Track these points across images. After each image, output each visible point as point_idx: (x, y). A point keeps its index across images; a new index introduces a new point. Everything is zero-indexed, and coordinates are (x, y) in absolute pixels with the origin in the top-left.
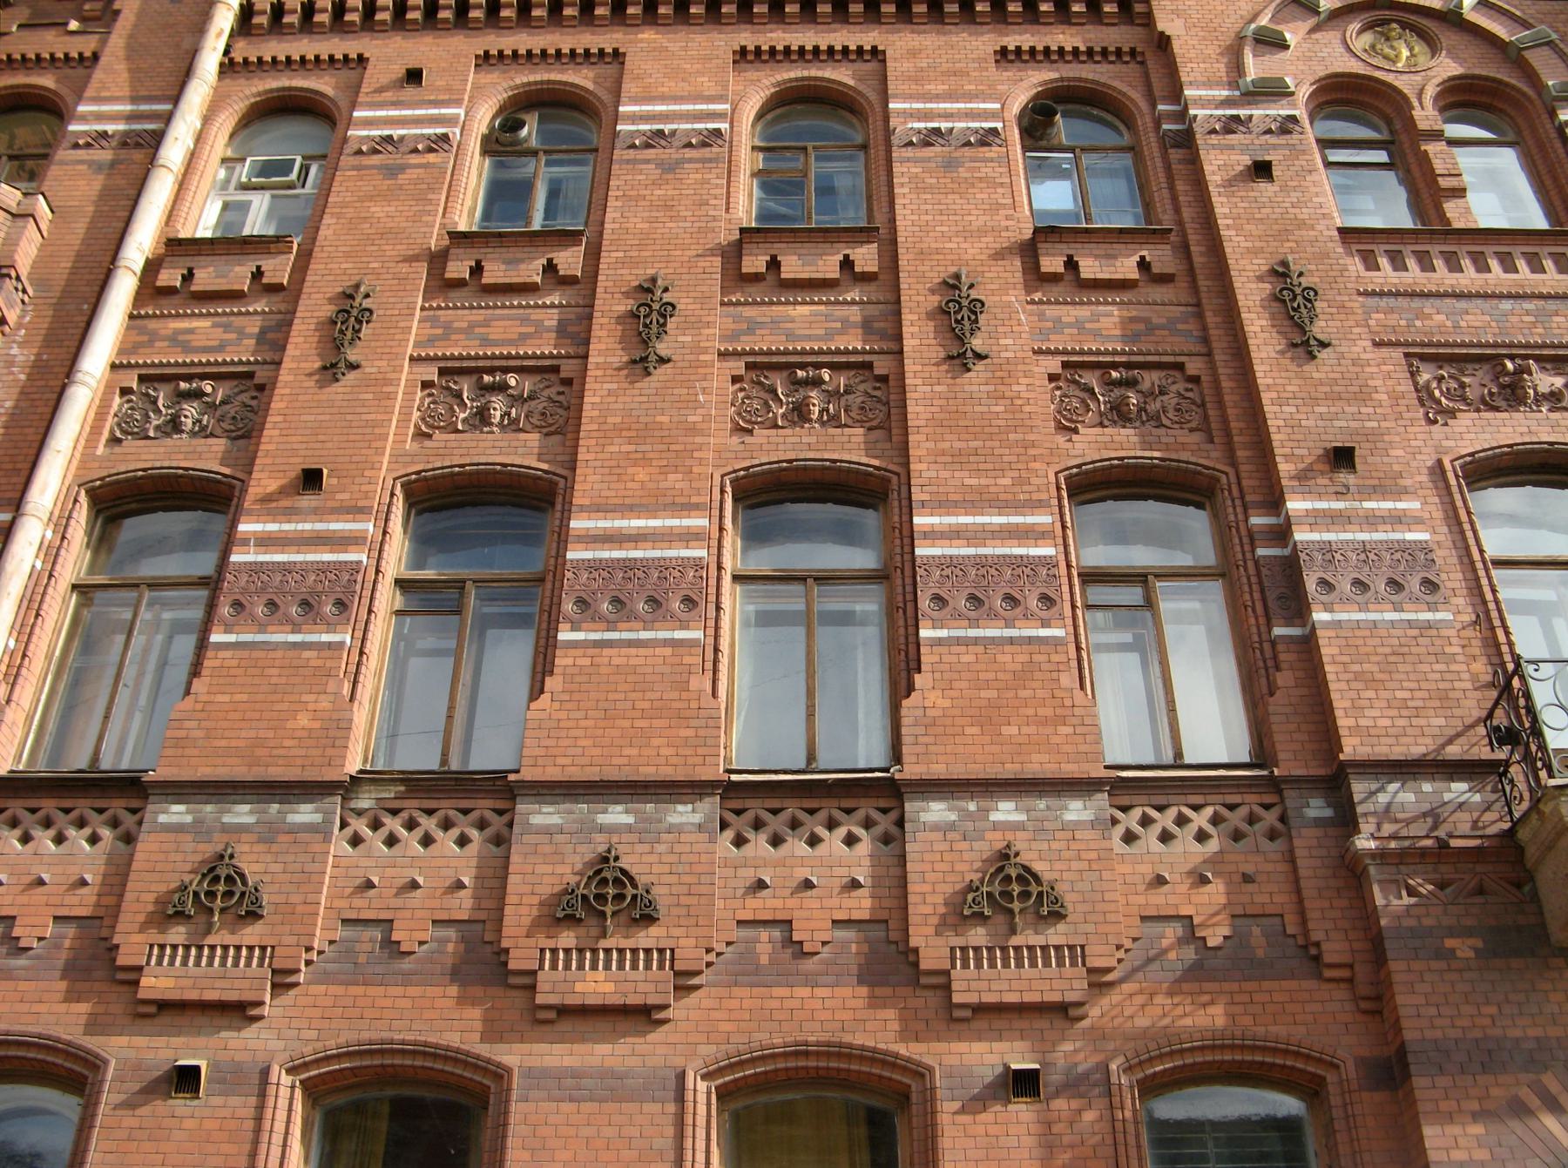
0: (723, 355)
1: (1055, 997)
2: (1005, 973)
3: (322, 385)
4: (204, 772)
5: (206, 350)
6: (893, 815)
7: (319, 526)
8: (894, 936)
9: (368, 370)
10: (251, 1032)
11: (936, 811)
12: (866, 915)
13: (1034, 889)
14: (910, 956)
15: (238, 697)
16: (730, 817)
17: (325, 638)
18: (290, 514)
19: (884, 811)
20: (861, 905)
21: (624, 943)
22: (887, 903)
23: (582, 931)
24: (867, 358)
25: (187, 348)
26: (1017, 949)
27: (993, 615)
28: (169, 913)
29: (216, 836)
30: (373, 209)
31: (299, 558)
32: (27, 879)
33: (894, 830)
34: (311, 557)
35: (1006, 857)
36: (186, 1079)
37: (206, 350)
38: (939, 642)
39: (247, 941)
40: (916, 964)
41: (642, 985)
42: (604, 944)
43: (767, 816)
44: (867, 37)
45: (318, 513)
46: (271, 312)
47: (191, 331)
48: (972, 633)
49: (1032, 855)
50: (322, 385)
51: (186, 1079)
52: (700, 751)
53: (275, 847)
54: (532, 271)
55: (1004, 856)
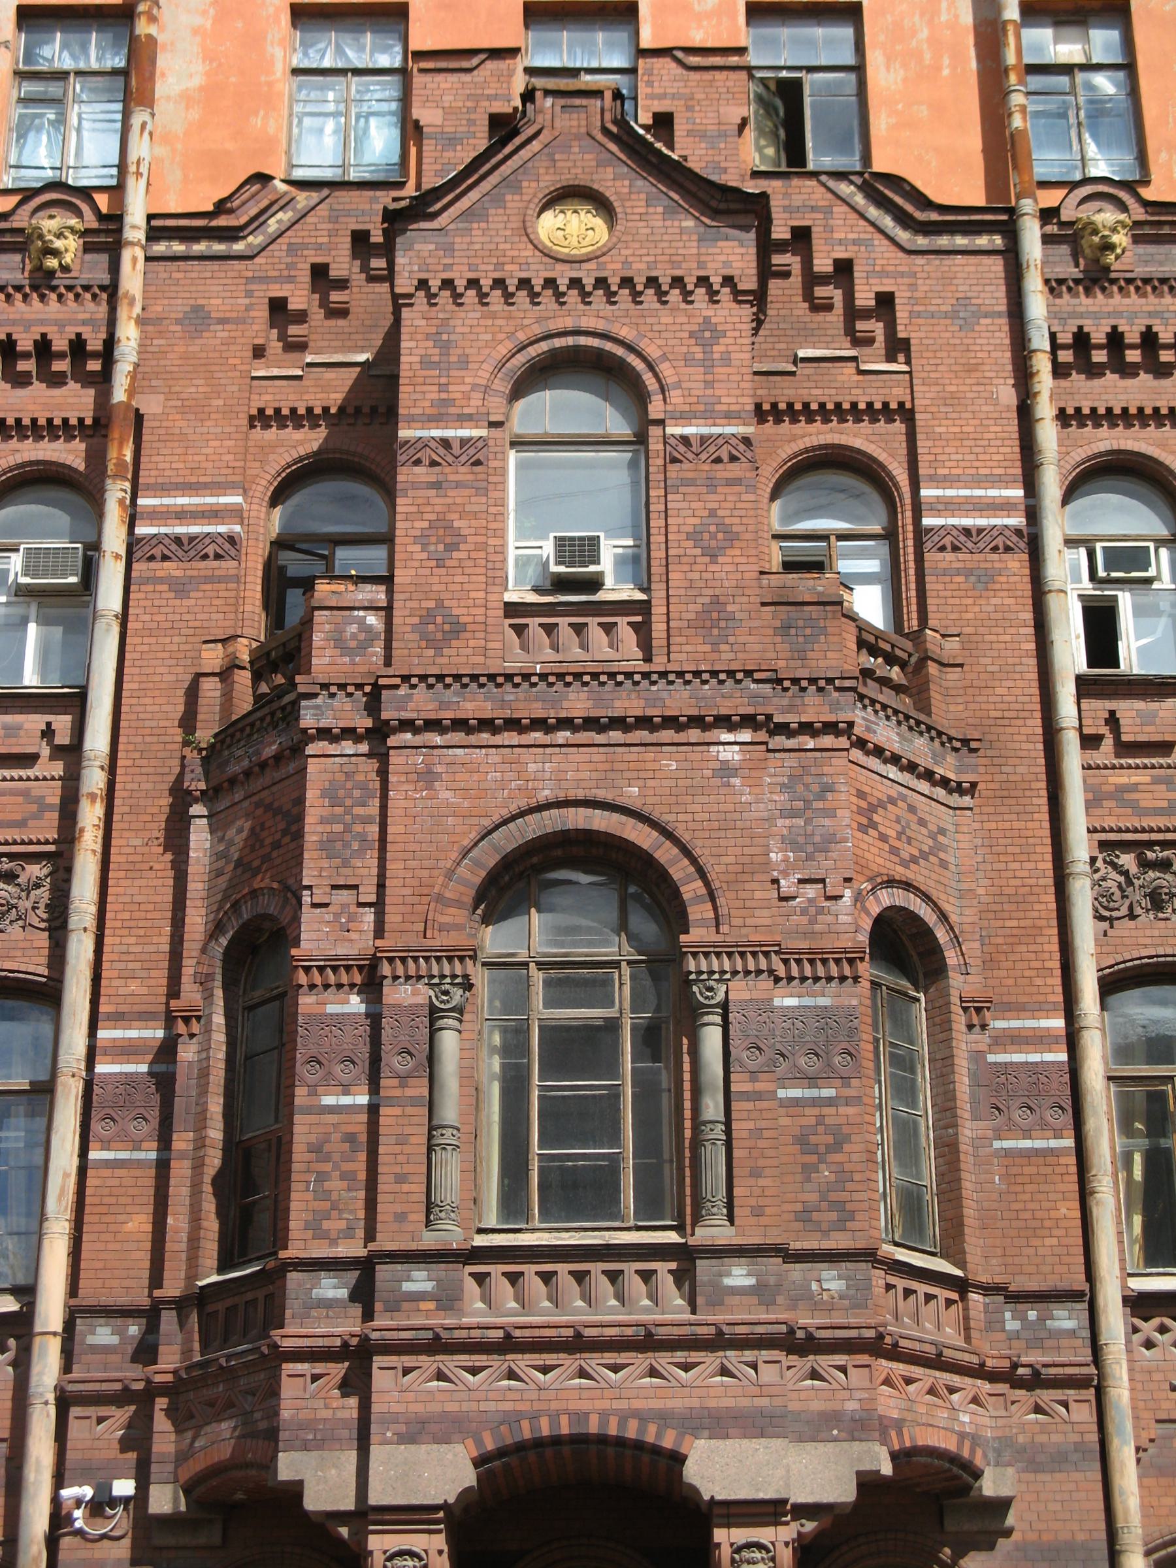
47: (1134, 788)
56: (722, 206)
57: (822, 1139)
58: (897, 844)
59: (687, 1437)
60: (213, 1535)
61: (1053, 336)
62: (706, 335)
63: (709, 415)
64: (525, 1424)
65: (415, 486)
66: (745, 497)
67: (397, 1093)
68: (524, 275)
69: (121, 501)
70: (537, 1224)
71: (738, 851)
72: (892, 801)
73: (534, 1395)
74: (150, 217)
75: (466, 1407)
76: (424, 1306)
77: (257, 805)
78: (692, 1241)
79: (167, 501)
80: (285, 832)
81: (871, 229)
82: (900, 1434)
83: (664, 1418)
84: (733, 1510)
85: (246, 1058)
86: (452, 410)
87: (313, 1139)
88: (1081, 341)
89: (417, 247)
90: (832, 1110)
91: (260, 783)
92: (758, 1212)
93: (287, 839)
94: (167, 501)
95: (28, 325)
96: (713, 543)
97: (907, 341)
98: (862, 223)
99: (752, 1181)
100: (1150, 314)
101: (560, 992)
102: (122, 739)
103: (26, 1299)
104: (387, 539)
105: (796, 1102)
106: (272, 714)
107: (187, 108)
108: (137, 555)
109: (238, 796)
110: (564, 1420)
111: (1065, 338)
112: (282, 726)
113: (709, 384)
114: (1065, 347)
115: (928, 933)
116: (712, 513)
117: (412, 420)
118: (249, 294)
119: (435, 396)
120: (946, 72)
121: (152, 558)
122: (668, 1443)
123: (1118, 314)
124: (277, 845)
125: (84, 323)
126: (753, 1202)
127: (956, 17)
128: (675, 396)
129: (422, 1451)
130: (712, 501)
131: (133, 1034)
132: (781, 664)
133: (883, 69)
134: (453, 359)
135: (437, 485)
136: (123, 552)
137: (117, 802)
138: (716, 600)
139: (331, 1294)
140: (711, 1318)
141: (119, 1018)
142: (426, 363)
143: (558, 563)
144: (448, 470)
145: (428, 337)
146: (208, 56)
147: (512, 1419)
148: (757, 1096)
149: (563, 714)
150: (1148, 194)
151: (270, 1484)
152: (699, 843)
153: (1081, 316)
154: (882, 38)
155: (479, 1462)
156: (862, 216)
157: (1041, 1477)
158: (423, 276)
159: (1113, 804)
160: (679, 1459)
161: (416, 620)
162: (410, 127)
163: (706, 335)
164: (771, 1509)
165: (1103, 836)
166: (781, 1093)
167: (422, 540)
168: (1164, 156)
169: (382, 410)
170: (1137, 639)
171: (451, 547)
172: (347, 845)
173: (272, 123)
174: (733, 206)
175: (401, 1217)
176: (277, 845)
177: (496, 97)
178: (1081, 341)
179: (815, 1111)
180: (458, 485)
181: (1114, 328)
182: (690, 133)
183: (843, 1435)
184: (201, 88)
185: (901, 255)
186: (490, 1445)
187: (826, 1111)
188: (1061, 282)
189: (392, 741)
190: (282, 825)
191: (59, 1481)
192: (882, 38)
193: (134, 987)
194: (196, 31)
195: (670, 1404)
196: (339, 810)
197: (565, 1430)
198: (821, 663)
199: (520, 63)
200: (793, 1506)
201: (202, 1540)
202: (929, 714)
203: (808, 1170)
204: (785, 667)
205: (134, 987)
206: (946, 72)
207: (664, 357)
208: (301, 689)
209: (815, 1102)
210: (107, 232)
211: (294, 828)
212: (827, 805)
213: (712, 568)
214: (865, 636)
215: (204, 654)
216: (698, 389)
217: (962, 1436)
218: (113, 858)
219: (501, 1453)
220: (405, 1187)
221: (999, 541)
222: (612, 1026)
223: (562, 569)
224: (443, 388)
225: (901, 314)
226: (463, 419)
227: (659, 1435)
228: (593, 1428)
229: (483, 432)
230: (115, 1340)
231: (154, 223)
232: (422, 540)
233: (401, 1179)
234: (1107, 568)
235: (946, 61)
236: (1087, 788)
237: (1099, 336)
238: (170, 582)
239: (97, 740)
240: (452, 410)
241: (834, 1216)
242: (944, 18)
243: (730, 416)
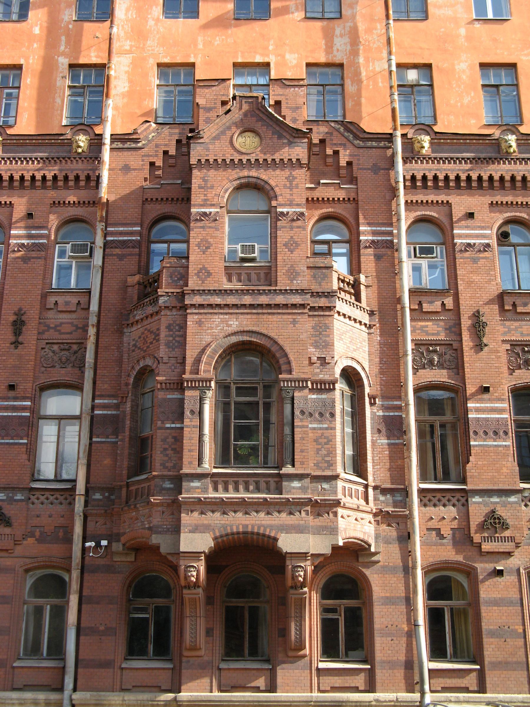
0: (503, 341)
1: (507, 550)
2: (505, 544)
3: (477, 352)
4: (501, 487)
5: (433, 334)
6: (465, 498)
7: (492, 405)
8: (466, 533)
9: (491, 346)
10: (512, 559)
11: (477, 499)
12: (456, 527)
13: (502, 521)
14: (471, 539)
15: (484, 463)
16: (423, 498)
17: (504, 443)
18: (481, 401)
19: (462, 497)
20: (455, 524)
21: (502, 535)
22: (463, 523)
23: (489, 532)
24: (451, 342)
25: (428, 334)
26: (498, 537)
27: (490, 438)
28: (482, 527)
29: (490, 505)
30: (474, 278)
31: (489, 416)
32: (439, 518)
33: (465, 503)
34: (493, 416)
35: (494, 512)
36: (500, 573)
37: (433, 334)
38: (476, 446)
39: (507, 535)
40: (472, 541)
41: (507, 547)
42: (497, 535)
43: (451, 498)
44: (442, 198)
45: (490, 400)
46: (450, 319)
47: (427, 326)
48: (485, 443)
49: (501, 512)
50: (477, 352)
51: (500, 573)
52: (22, 472)
53: (507, 508)
54: (437, 306)
55: (493, 512)
56: (297, 135)
57: (323, 441)
58: (349, 345)
59: (279, 533)
60: (131, 558)
61: (404, 177)
62: (291, 179)
63: (291, 205)
64: (229, 528)
65: (196, 227)
66: (302, 232)
67: (189, 424)
68: (232, 158)
69: (102, 229)
70: (233, 465)
71: (298, 348)
72: (347, 331)
73: (232, 519)
74: (112, 135)
75: (210, 522)
76: (197, 490)
77: (146, 329)
78: (281, 472)
79: (116, 229)
80: (154, 339)
81: (345, 140)
82: (345, 533)
83: (271, 527)
84: (293, 555)
85: (142, 410)
86: (208, 203)
87: (163, 437)
88: (413, 178)
89: (198, 148)
90: (326, 431)
91: (145, 322)
92: (302, 463)
93: (155, 341)
94: (116, 229)
95: (72, 170)
96: (292, 247)
97: (356, 178)
98: (343, 138)
99: (301, 454)
100: (437, 170)
101: (241, 391)
102: (102, 307)
103: (74, 484)
104: (187, 242)
105: (314, 429)
106: (150, 301)
107: (123, 98)
108: (107, 246)
109: (139, 326)
110: (241, 527)
111: (408, 177)
112: (153, 305)
113: (291, 195)
114: (408, 180)
115: (358, 374)
116: (292, 237)
117: (195, 205)
118: (143, 161)
119: (203, 198)
120: (371, 87)
121: (112, 248)
122: (272, 534)
123: (424, 169)
124: (151, 343)
125: (90, 170)
126: (301, 460)
127: (375, 68)
128: (280, 199)
129: (197, 535)
130: (292, 233)
131: (106, 401)
132: (312, 287)
133: (350, 86)
134: (209, 186)
135: (203, 227)
136: (102, 246)
137: (101, 327)
138: (292, 266)
139: (168, 486)
140: (287, 496)
141: (101, 396)
142: (200, 187)
143: (242, 253)
144: (207, 222)
145: (201, 178)
146: (130, 81)
147: (224, 527)
148: (302, 427)
149: (243, 303)
150: (436, 129)
151: (150, 544)
152: (285, 345)
153: (414, 170)
154: (350, 75)
155: (215, 539)
156: (343, 136)
157: (390, 545)
158: (199, 158)
159: (419, 331)
160: (276, 540)
161: (196, 272)
162: (195, 105)
163: (291, 179)
164: (304, 555)
165: (416, 342)
166: (310, 426)
167: (199, 245)
168: (442, 116)
169: (185, 199)
170: (429, 276)
171: (208, 248)
172: (174, 344)
173: (150, 103)
174: (300, 135)
175: (190, 463)
176: (151, 343)
177: (223, 95)
178: (413, 178)
179: (322, 431)
180: (210, 227)
181: (424, 174)
182: (287, 108)
183: (328, 533)
184: (128, 92)
185: (355, 149)
186: (218, 534)
187: (325, 431)
188: (407, 158)
189: (188, 311)
190: (153, 337)
191: (85, 539)
192: (350, 75)
193: (106, 386)
194: (126, 72)
195: (273, 522)
196: (171, 333)
197: (241, 530)
198: (326, 287)
199: (232, 82)
200: (312, 555)
201: (129, 560)
202: (360, 303)
203: (318, 450)
204: (315, 288)
205: (106, 386)
206: (371, 87)
207: (277, 186)
208: (159, 294)
209: (321, 429)
210: (97, 139)
211: (157, 338)
212: (327, 333)
213: (291, 255)
214: (341, 277)
215: (128, 280)
216: (288, 196)
217: (365, 533)
218: (100, 345)
219: (221, 536)
220: (192, 453)
221: (385, 245)
222: (257, 403)
223: (243, 255)
224: (205, 195)
225: (355, 167)
226: (213, 205)
227: (270, 532)
228: (250, 529)
229: (218, 210)
230: (101, 497)
231: (113, 137)
232: (199, 245)
233: (190, 451)
234: (420, 254)
235: (371, 83)
236: (411, 326)
237: (419, 177)
238: (117, 255)
239: (94, 307)
240: (208, 203)
241: (326, 465)
242: (371, 68)
243: (298, 205)
